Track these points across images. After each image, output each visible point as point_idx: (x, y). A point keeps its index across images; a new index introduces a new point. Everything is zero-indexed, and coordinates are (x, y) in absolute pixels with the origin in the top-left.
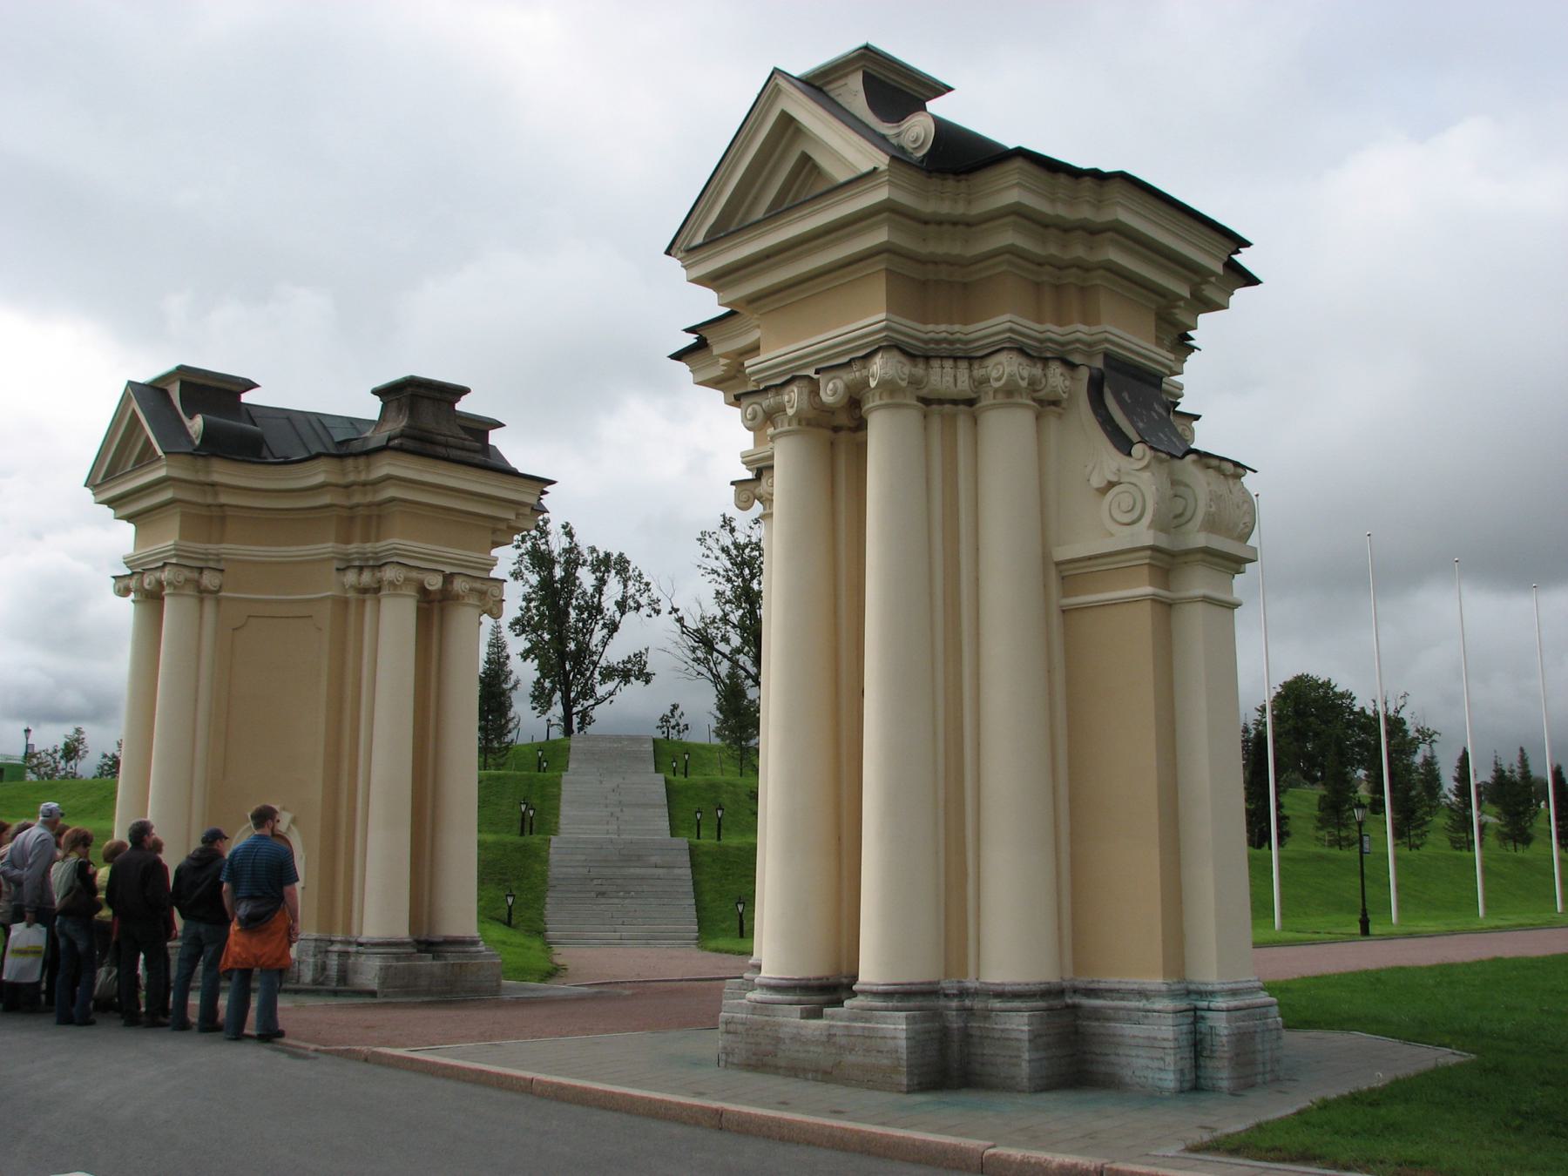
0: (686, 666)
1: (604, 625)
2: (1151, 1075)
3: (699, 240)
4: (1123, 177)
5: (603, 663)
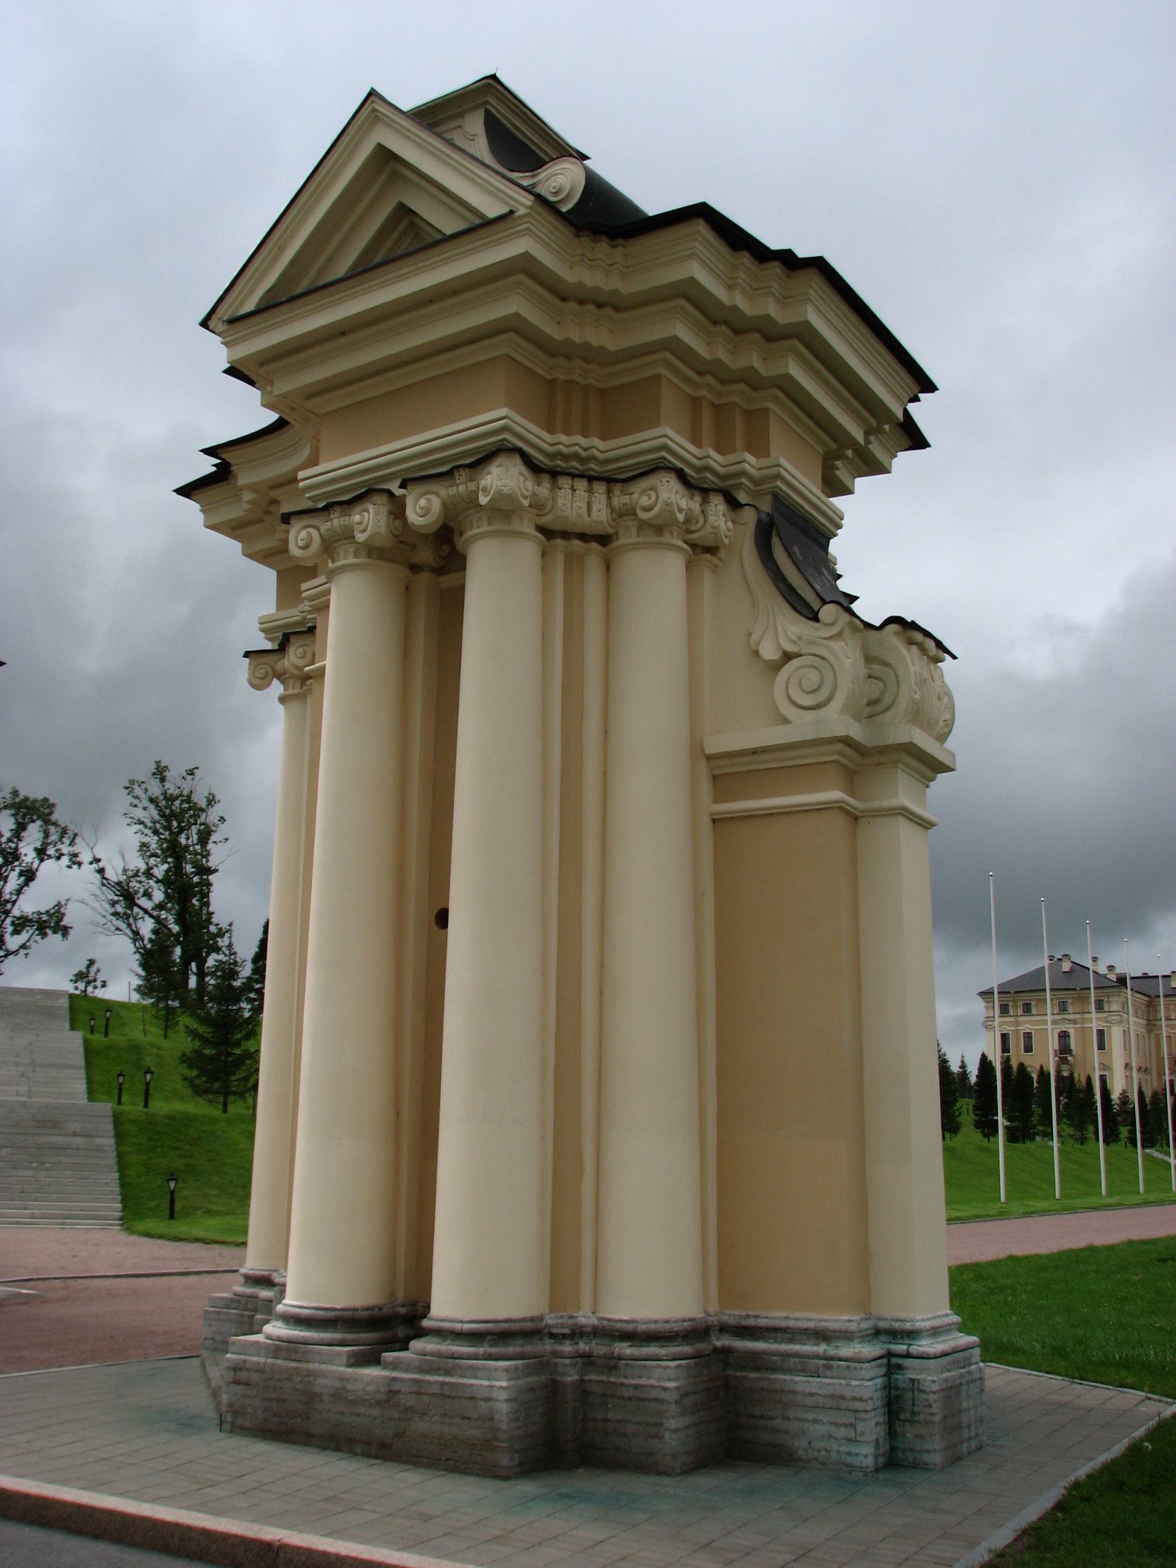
0: (104, 921)
1: (21, 874)
2: (835, 1448)
3: (250, 306)
4: (820, 265)
5: (16, 912)
